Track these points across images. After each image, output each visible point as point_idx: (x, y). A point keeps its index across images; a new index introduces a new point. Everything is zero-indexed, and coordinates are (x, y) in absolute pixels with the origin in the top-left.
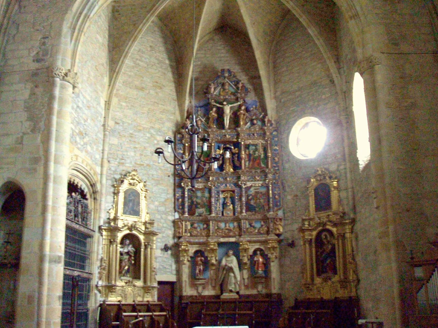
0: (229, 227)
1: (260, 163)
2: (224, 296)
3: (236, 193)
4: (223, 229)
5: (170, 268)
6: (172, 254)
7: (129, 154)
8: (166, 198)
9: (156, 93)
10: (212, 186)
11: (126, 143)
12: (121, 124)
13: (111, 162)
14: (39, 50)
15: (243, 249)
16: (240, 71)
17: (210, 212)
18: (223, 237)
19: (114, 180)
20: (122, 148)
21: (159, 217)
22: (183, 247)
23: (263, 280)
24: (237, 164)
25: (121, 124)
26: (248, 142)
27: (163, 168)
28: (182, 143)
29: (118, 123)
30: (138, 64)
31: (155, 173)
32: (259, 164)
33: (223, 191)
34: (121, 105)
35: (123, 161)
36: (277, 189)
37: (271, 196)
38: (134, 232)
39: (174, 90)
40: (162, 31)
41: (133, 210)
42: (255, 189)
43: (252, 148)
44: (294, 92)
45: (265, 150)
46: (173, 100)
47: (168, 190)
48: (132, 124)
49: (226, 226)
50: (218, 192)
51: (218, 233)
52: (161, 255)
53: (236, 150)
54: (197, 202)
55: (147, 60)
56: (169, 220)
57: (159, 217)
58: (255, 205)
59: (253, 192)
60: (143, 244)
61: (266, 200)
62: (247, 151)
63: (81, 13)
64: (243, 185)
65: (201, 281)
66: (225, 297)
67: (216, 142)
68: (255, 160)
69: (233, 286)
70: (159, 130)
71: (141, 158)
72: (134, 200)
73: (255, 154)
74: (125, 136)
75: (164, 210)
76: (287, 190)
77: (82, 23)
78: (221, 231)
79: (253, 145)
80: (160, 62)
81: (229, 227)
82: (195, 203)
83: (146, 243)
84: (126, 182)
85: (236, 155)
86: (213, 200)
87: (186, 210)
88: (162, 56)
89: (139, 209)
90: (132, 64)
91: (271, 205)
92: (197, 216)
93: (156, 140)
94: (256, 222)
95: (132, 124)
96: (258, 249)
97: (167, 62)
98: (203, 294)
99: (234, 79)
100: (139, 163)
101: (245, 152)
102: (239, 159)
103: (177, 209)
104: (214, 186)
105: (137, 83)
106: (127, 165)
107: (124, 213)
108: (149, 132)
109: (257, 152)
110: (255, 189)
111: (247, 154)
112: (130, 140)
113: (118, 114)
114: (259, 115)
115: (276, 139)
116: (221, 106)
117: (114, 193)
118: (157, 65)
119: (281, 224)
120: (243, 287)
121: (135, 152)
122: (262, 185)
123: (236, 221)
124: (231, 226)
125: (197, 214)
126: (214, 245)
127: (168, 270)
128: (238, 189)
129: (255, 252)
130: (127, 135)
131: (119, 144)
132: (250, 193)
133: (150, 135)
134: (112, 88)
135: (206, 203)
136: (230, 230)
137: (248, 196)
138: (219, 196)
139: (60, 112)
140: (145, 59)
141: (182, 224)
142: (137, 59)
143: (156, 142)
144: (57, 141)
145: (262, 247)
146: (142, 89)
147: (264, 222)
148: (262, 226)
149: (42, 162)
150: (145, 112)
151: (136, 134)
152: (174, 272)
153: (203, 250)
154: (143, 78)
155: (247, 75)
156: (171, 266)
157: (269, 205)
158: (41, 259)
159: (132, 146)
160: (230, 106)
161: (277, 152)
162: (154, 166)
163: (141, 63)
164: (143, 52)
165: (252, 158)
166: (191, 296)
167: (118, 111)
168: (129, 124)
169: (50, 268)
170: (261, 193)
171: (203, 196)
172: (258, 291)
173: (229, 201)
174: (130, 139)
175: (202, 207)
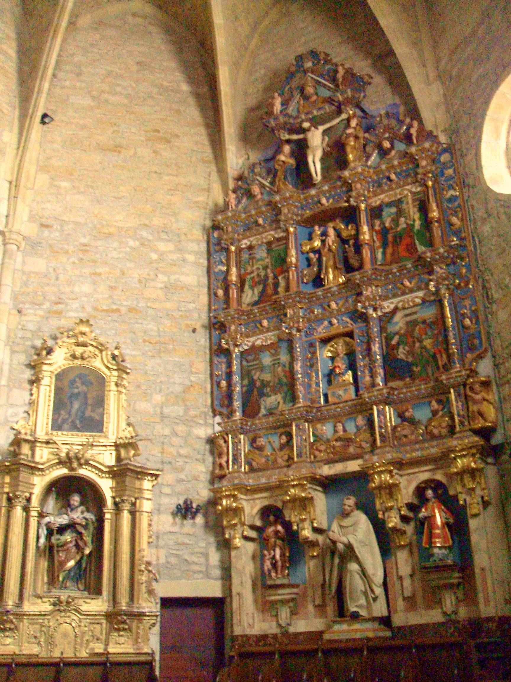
0: (345, 431)
1: (415, 245)
3: (356, 336)
4: (328, 441)
5: (202, 560)
6: (206, 525)
7: (77, 289)
8: (188, 383)
9: (155, 152)
10: (294, 332)
11: (69, 268)
12: (57, 226)
13: (24, 311)
15: (380, 488)
16: (351, 53)
17: (294, 398)
18: (330, 462)
19: (33, 351)
20: (57, 279)
21: (167, 431)
22: (224, 502)
23: (455, 577)
24: (354, 262)
25: (57, 226)
26: (376, 202)
27: (177, 314)
28: (222, 249)
29: (47, 226)
31: (152, 326)
32: (411, 248)
33: (325, 341)
34: (59, 187)
35: (60, 306)
36: (467, 303)
37: (449, 322)
38: (84, 472)
39: (206, 142)
40: (169, 31)
42: (406, 315)
43: (389, 213)
45: (423, 208)
46: (204, 162)
47: (191, 365)
49: (336, 431)
50: (312, 345)
51: (317, 453)
52: (176, 529)
53: (348, 231)
54: (262, 381)
56: (199, 438)
57: (167, 431)
58: (410, 359)
59: (401, 324)
60: (109, 502)
62: (377, 222)
64: (371, 311)
65: (281, 591)
66: (335, 637)
67: (298, 223)
68: (398, 238)
69: (363, 601)
71: (111, 297)
72: (85, 394)
73: (397, 225)
74: (67, 252)
75: (181, 413)
76: (496, 296)
78: (323, 448)
79: (390, 205)
81: (345, 431)
82: (258, 384)
83: (117, 500)
85: (351, 242)
86: (298, 367)
87: (237, 404)
90: (88, 102)
91: (454, 349)
92: (264, 416)
94: (415, 406)
96: (426, 482)
97: (185, 87)
98: (291, 630)
99: (327, 67)
100: (105, 308)
101: (372, 227)
102: (358, 247)
103: (218, 408)
104: (299, 330)
107: (57, 426)
109: (402, 220)
110: (406, 315)
112: (81, 260)
113: (48, 205)
114: (398, 127)
115: (450, 172)
116: (301, 136)
117: (32, 382)
119: (490, 397)
120: (400, 604)
122: (424, 301)
123: (361, 412)
124: (351, 427)
125: (263, 411)
126: (302, 486)
127: (196, 568)
128: (362, 325)
129: (420, 491)
130: (71, 248)
131: (51, 270)
132: (391, 329)
133: (137, 243)
134: (23, 152)
135: (285, 380)
136: (348, 441)
137: (388, 339)
138: (314, 353)
140: (124, 88)
141: (226, 442)
142: (103, 91)
145: (439, 476)
146: (117, 149)
147: (439, 402)
148: (435, 413)
152: (217, 572)
153: (279, 504)
154: (118, 126)
155: (368, 54)
156: (206, 556)
157: (447, 350)
159: (87, 271)
160: (321, 128)
161: (456, 204)
162: (150, 311)
165: (390, 237)
166: (264, 637)
167: (49, 202)
170: (424, 322)
171: (276, 363)
172: (445, 613)
173: (341, 364)
174: (81, 255)
175: (275, 391)
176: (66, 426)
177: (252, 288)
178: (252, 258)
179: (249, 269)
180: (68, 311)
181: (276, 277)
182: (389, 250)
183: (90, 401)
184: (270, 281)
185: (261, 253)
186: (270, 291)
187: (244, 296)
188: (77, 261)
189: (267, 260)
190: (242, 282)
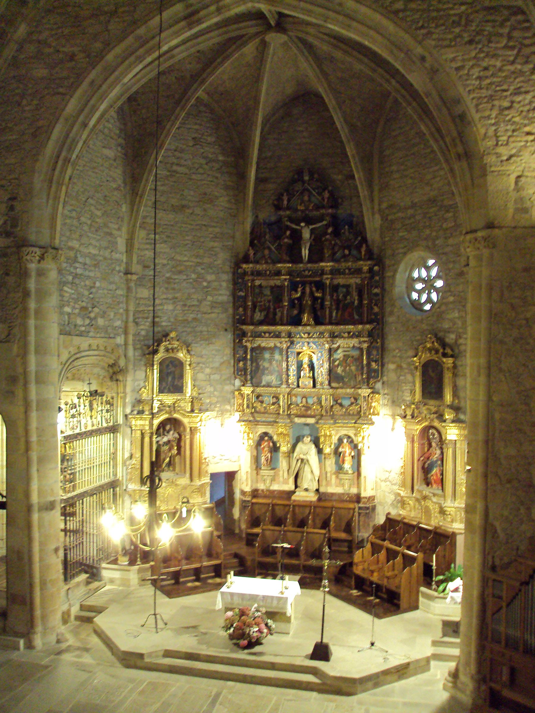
0: (307, 402)
1: (353, 314)
2: (299, 496)
14: (6, 218)
30: (176, 172)
38: (176, 416)
41: (173, 386)
42: (344, 351)
44: (406, 208)
48: (168, 264)
55: (189, 163)
58: (343, 374)
61: (360, 368)
62: (335, 295)
63: (58, 157)
68: (346, 307)
70: (210, 266)
72: (174, 372)
77: (61, 173)
79: (344, 286)
80: (209, 161)
81: (307, 402)
84: (162, 349)
88: (212, 150)
89: (183, 383)
93: (205, 280)
95: (168, 264)
101: (332, 296)
105: (174, 202)
106: (164, 324)
107: (161, 391)
108: (194, 272)
110: (344, 351)
111: (334, 300)
118: (205, 166)
121: (174, 303)
122: (354, 347)
129: (340, 440)
139: (38, 312)
143: (205, 284)
144: (37, 352)
149: (21, 382)
150: (189, 242)
151: (176, 277)
158: (29, 509)
160: (311, 227)
163: (179, 169)
164: (182, 151)
165: (341, 305)
168: (164, 265)
169: (40, 519)
170: (352, 357)
174: (166, 286)
176: (166, 391)
177: (261, 311)
178: (261, 293)
180: (162, 322)
181: (275, 309)
182: (340, 313)
183: (176, 376)
184: (272, 310)
185: (267, 292)
186: (271, 316)
187: (255, 315)
188: (165, 290)
189: (270, 298)
190: (254, 306)
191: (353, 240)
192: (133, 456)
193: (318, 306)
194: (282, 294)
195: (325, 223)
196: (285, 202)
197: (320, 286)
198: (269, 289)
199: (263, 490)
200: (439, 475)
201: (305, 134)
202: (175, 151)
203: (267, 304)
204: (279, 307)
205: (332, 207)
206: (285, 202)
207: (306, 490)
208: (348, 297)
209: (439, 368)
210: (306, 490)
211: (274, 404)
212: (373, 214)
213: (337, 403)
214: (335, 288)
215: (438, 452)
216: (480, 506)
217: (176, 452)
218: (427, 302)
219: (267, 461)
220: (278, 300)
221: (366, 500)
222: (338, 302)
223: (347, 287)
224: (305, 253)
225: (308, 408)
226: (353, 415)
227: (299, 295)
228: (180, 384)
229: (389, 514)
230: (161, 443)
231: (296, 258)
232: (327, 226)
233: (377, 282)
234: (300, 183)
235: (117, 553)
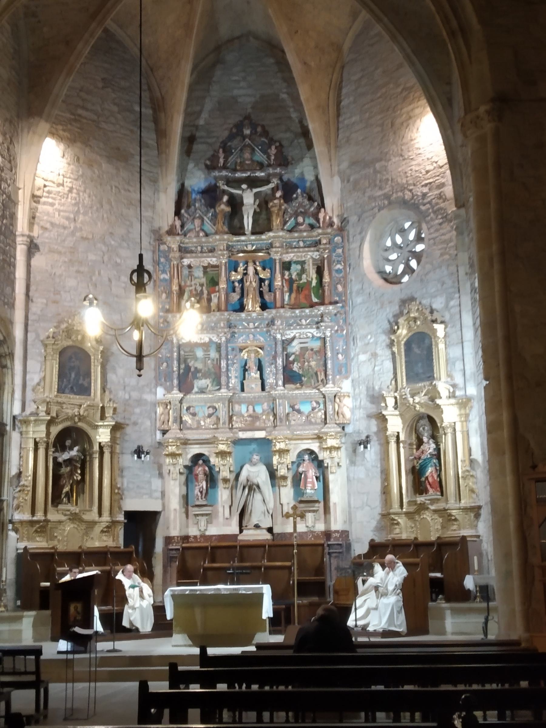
0: (254, 411)
2: (247, 535)
42: (301, 343)
43: (295, 269)
58: (301, 373)
62: (287, 273)
68: (300, 289)
81: (254, 411)
101: (283, 275)
110: (301, 343)
115: (340, 251)
129: (300, 455)
132: (290, 350)
165: (295, 285)
170: (312, 350)
178: (191, 275)
179: (188, 283)
182: (293, 295)
185: (199, 273)
191: (307, 207)
192: (23, 475)
193: (265, 288)
194: (219, 275)
195: (271, 186)
196: (222, 161)
197: (268, 264)
198: (202, 269)
199: (195, 537)
200: (435, 476)
201: (242, 84)
202: (81, 91)
203: (199, 289)
204: (215, 292)
205: (280, 165)
206: (222, 161)
207: (257, 527)
208: (304, 276)
209: (427, 341)
210: (257, 527)
211: (210, 416)
212: (332, 176)
213: (294, 409)
214: (286, 266)
215: (433, 446)
216: (505, 416)
217: (79, 478)
218: (404, 273)
219: (201, 492)
220: (214, 282)
221: (338, 535)
222: (291, 282)
223: (302, 263)
224: (248, 222)
225: (255, 417)
226: (316, 423)
227: (239, 277)
228: (86, 385)
229: (372, 540)
230: (60, 460)
231: (238, 230)
232: (274, 190)
233: (339, 256)
234: (239, 138)
235: (160, 317)
